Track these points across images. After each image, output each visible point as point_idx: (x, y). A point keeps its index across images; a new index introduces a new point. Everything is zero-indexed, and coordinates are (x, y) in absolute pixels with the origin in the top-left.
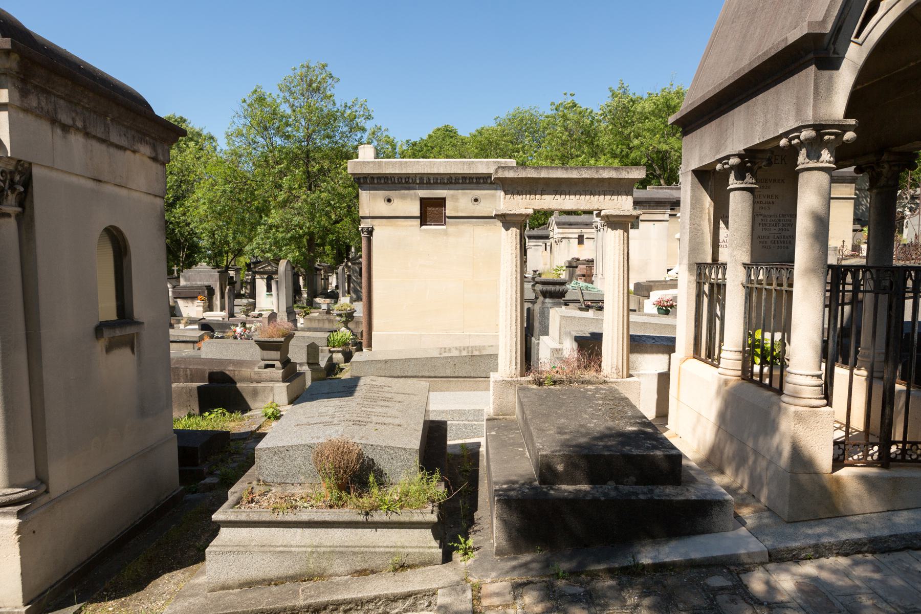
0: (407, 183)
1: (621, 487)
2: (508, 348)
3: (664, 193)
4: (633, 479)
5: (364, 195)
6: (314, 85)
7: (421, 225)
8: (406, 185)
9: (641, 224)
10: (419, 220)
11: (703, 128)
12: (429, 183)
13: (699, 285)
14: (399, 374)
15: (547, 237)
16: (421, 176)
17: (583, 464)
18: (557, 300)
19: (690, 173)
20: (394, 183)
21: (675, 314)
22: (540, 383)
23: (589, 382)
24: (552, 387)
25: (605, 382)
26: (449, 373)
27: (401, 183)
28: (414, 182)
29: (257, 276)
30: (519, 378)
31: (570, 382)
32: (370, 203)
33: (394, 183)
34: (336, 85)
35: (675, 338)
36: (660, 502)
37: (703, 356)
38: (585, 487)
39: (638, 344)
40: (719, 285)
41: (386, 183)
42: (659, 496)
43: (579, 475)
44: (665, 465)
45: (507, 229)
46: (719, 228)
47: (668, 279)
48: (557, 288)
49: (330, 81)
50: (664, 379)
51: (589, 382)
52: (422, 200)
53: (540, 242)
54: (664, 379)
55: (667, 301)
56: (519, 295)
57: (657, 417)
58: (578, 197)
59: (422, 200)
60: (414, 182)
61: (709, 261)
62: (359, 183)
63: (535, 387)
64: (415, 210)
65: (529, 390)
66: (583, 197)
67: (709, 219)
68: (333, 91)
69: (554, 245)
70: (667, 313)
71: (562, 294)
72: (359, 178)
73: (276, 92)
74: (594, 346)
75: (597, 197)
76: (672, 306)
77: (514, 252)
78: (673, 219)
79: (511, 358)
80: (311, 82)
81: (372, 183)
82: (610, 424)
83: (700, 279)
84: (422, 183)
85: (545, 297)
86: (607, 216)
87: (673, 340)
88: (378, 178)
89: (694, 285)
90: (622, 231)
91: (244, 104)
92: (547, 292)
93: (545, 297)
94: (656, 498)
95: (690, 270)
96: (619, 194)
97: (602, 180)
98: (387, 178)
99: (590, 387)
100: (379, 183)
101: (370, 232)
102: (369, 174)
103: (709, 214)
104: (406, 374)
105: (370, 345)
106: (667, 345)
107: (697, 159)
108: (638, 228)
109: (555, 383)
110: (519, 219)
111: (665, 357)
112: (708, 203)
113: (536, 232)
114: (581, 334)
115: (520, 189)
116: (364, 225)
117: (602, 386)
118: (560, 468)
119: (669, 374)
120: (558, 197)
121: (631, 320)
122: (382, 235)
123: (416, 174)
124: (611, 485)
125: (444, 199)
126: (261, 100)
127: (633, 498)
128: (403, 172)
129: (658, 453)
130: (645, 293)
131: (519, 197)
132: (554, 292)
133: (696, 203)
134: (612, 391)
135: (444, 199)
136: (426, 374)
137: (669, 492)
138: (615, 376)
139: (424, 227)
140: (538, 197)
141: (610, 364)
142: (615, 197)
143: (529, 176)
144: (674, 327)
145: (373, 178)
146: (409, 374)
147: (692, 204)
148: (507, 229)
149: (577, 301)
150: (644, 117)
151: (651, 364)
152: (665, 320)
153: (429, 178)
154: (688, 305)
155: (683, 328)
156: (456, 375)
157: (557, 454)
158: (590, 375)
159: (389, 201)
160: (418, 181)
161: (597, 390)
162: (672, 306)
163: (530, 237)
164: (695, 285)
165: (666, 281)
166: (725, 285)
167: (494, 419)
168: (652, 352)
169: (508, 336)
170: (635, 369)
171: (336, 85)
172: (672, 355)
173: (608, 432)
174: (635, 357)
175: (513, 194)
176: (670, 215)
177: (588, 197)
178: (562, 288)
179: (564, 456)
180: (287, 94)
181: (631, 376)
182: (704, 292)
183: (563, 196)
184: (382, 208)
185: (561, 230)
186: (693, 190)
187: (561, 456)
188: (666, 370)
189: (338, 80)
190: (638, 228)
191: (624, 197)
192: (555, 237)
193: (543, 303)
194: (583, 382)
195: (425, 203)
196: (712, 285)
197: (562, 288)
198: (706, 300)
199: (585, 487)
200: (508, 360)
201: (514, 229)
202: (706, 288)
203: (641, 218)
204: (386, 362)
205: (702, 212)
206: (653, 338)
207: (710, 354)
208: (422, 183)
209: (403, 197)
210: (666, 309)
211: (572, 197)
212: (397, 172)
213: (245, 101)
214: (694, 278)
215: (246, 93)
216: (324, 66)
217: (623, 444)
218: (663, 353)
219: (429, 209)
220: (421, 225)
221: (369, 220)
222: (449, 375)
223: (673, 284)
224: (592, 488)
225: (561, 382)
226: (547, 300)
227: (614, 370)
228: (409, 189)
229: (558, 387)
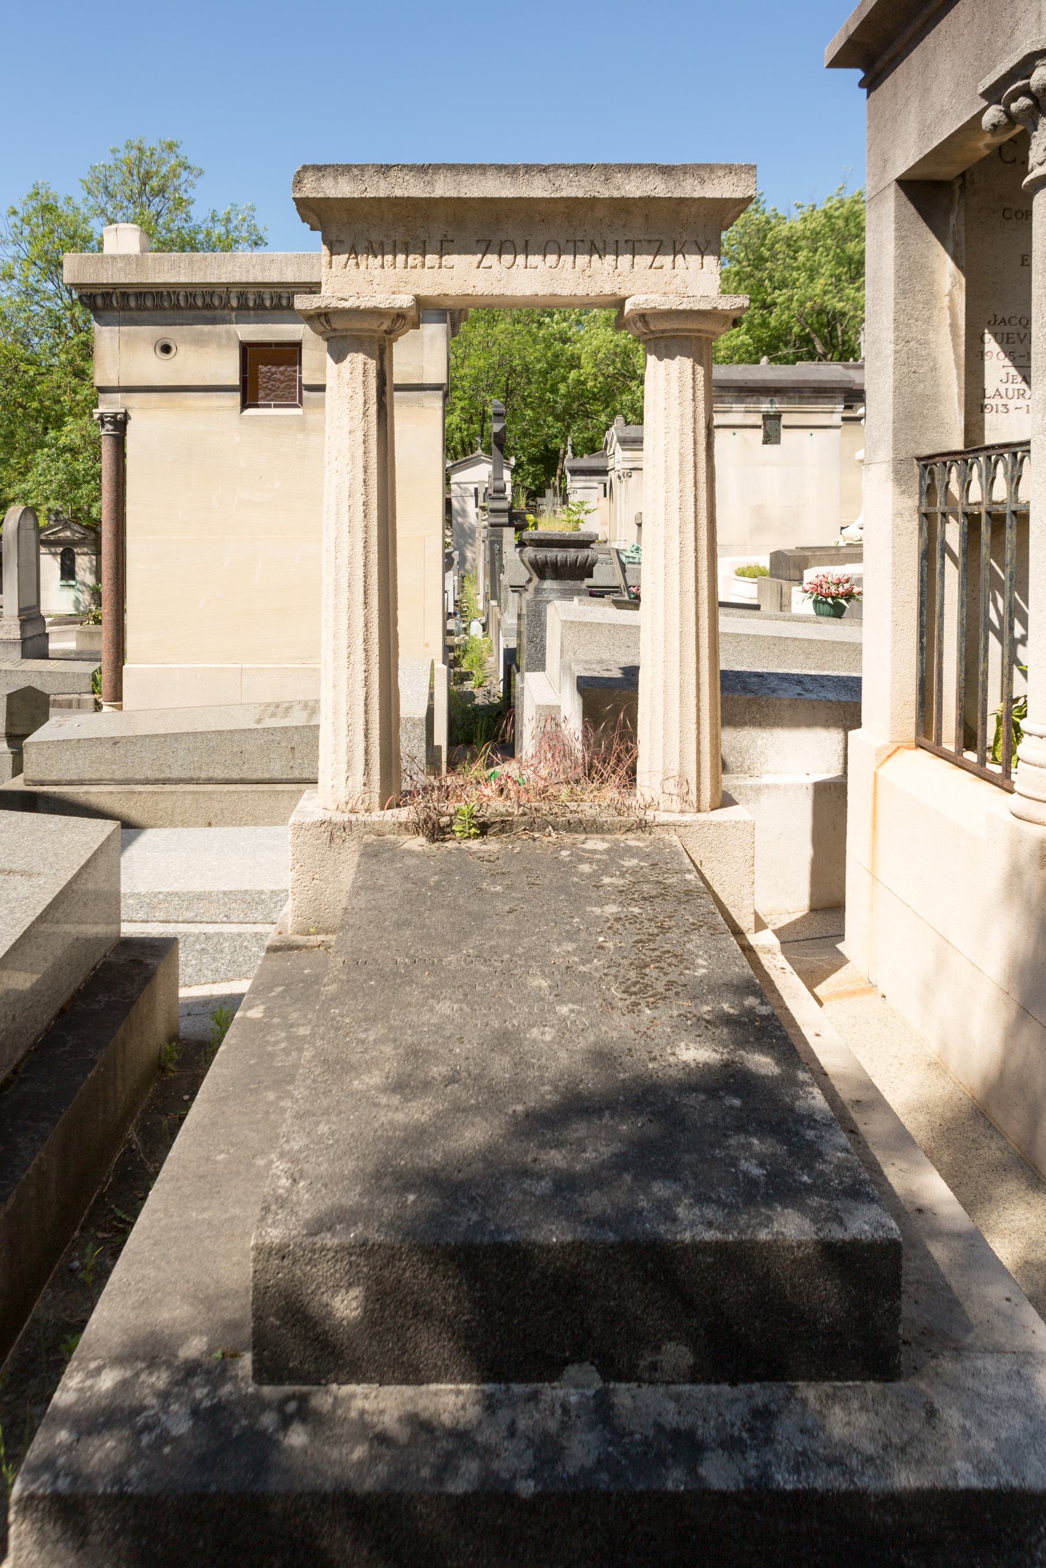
0: (208, 307)
1: (624, 1394)
2: (343, 720)
3: (829, 371)
4: (677, 1354)
5: (108, 339)
6: (155, 183)
7: (245, 406)
8: (205, 312)
9: (785, 434)
10: (237, 396)
11: (929, 40)
12: (260, 306)
13: (929, 523)
14: (150, 775)
15: (604, 472)
16: (242, 289)
17: (445, 1293)
18: (571, 583)
19: (894, 186)
20: (178, 307)
21: (858, 616)
22: (437, 832)
23: (594, 827)
24: (474, 844)
25: (643, 826)
26: (276, 771)
27: (193, 307)
28: (226, 306)
29: (43, 550)
30: (377, 816)
31: (531, 826)
32: (122, 354)
33: (178, 307)
34: (196, 182)
35: (859, 680)
36: (801, 1502)
37: (949, 744)
38: (450, 1399)
39: (746, 698)
40: (997, 520)
41: (158, 307)
42: (801, 1462)
43: (431, 1344)
44: (827, 1295)
45: (339, 358)
46: (982, 355)
47: (842, 544)
48: (572, 554)
49: (185, 175)
50: (830, 799)
51: (594, 827)
52: (247, 349)
53: (595, 481)
54: (830, 799)
55: (838, 583)
56: (374, 557)
57: (813, 910)
58: (552, 259)
59: (247, 349)
60: (226, 306)
61: (957, 443)
62: (94, 309)
63: (417, 843)
64: (229, 371)
65: (395, 853)
66: (567, 259)
67: (953, 326)
68: (192, 193)
69: (616, 483)
70: (838, 612)
71: (585, 570)
72: (92, 297)
73: (79, 196)
74: (616, 712)
75: (610, 258)
76: (849, 596)
77: (359, 425)
78: (851, 427)
79: (350, 749)
80: (148, 175)
81: (125, 308)
82: (618, 1028)
83: (931, 503)
84: (243, 307)
85: (542, 577)
86: (643, 317)
87: (853, 686)
88: (138, 295)
89: (912, 526)
90: (688, 363)
91: (14, 219)
92: (545, 563)
93: (542, 577)
94: (785, 1480)
95: (899, 477)
96: (676, 249)
97: (622, 206)
98: (160, 294)
99: (596, 844)
100: (140, 308)
101: (120, 424)
102: (115, 286)
103: (952, 309)
104: (167, 774)
105: (117, 696)
106: (836, 702)
107: (913, 137)
108: (778, 442)
109: (483, 829)
110: (372, 324)
111: (831, 737)
112: (947, 277)
113: (587, 461)
114: (597, 672)
115: (375, 236)
116: (109, 405)
117: (632, 840)
118: (346, 1305)
119: (810, 988)
120: (491, 259)
121: (721, 629)
122: (149, 428)
123: (228, 286)
124: (573, 1388)
125: (297, 345)
126: (48, 208)
127: (674, 1480)
128: (197, 279)
129: (791, 1227)
130: (794, 573)
131: (375, 262)
132: (564, 564)
133: (911, 277)
134: (660, 860)
135: (297, 345)
136: (219, 773)
137: (843, 1417)
138: (676, 805)
139: (250, 412)
140: (431, 259)
141: (659, 767)
142: (666, 260)
143: (398, 193)
144: (855, 649)
145: (125, 295)
146: (175, 775)
147: (900, 279)
148: (339, 358)
149: (614, 590)
150: (792, 244)
151: (790, 758)
152: (832, 630)
153: (260, 296)
154: (896, 584)
155: (882, 654)
156: (296, 774)
157: (329, 1240)
158: (598, 801)
159: (166, 349)
160: (234, 303)
161: (616, 852)
162: (849, 596)
163: (575, 472)
164: (915, 524)
165: (837, 548)
166: (1022, 518)
167: (291, 947)
168: (796, 723)
169: (343, 683)
170: (748, 771)
171: (196, 182)
172: (851, 733)
173: (592, 1081)
174: (742, 740)
175: (354, 251)
176: (844, 419)
177: (582, 260)
178: (582, 554)
179: (364, 1249)
180: (102, 199)
181: (725, 801)
182: (946, 548)
183: (507, 258)
184: (150, 367)
185: (629, 454)
186: (902, 238)
187: (341, 1248)
188: (835, 772)
189: (201, 173)
190: (778, 442)
191: (694, 260)
192: (618, 467)
193: (538, 591)
194: (570, 827)
195: (251, 355)
196: (972, 522)
197: (582, 554)
198: (952, 576)
199: (450, 1399)
200: (343, 758)
201: (360, 357)
202: (953, 533)
203: (785, 420)
204: (115, 742)
205: (930, 303)
206: (798, 680)
207: (969, 738)
208: (243, 307)
209: (200, 342)
210: (837, 604)
211: (535, 259)
212: (183, 279)
213: (15, 213)
214: (911, 503)
215: (18, 196)
216: (171, 147)
217: (644, 1160)
218: (827, 725)
219: (263, 369)
220: (245, 406)
221: (119, 395)
222: (277, 775)
223: (853, 553)
224: (490, 1405)
225: (504, 826)
226: (548, 584)
227: (671, 786)
228: (213, 321)
229: (492, 845)
